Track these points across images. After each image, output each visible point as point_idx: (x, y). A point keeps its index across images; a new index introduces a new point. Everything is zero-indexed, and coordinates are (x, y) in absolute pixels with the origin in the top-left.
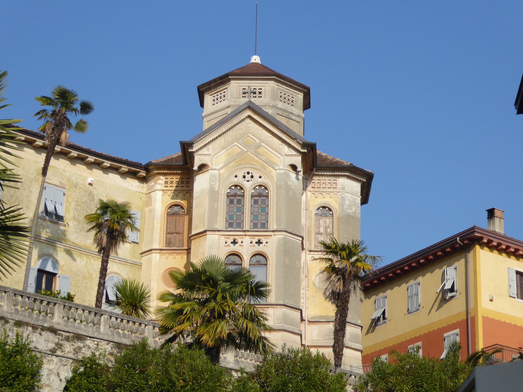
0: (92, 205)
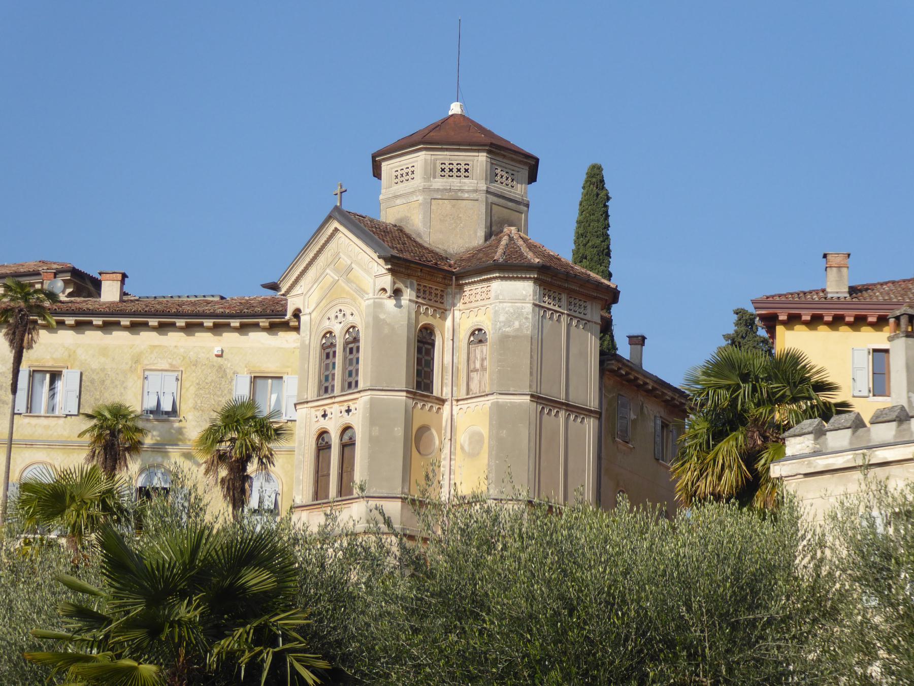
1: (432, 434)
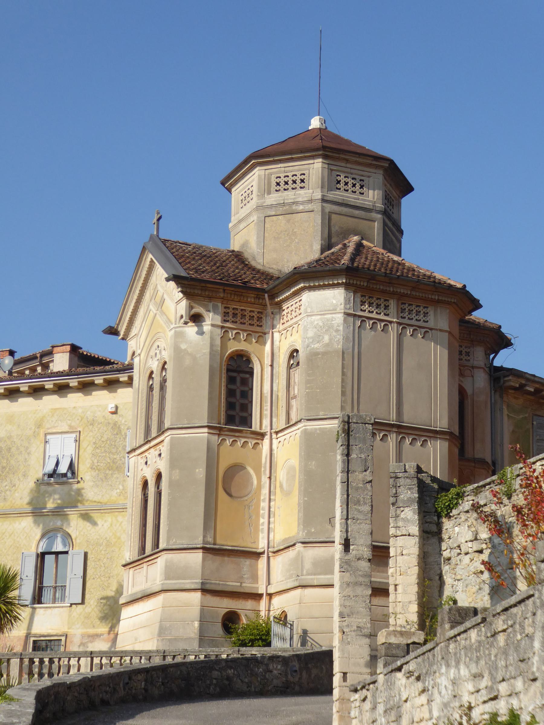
0: (118, 440)
1: (249, 473)
